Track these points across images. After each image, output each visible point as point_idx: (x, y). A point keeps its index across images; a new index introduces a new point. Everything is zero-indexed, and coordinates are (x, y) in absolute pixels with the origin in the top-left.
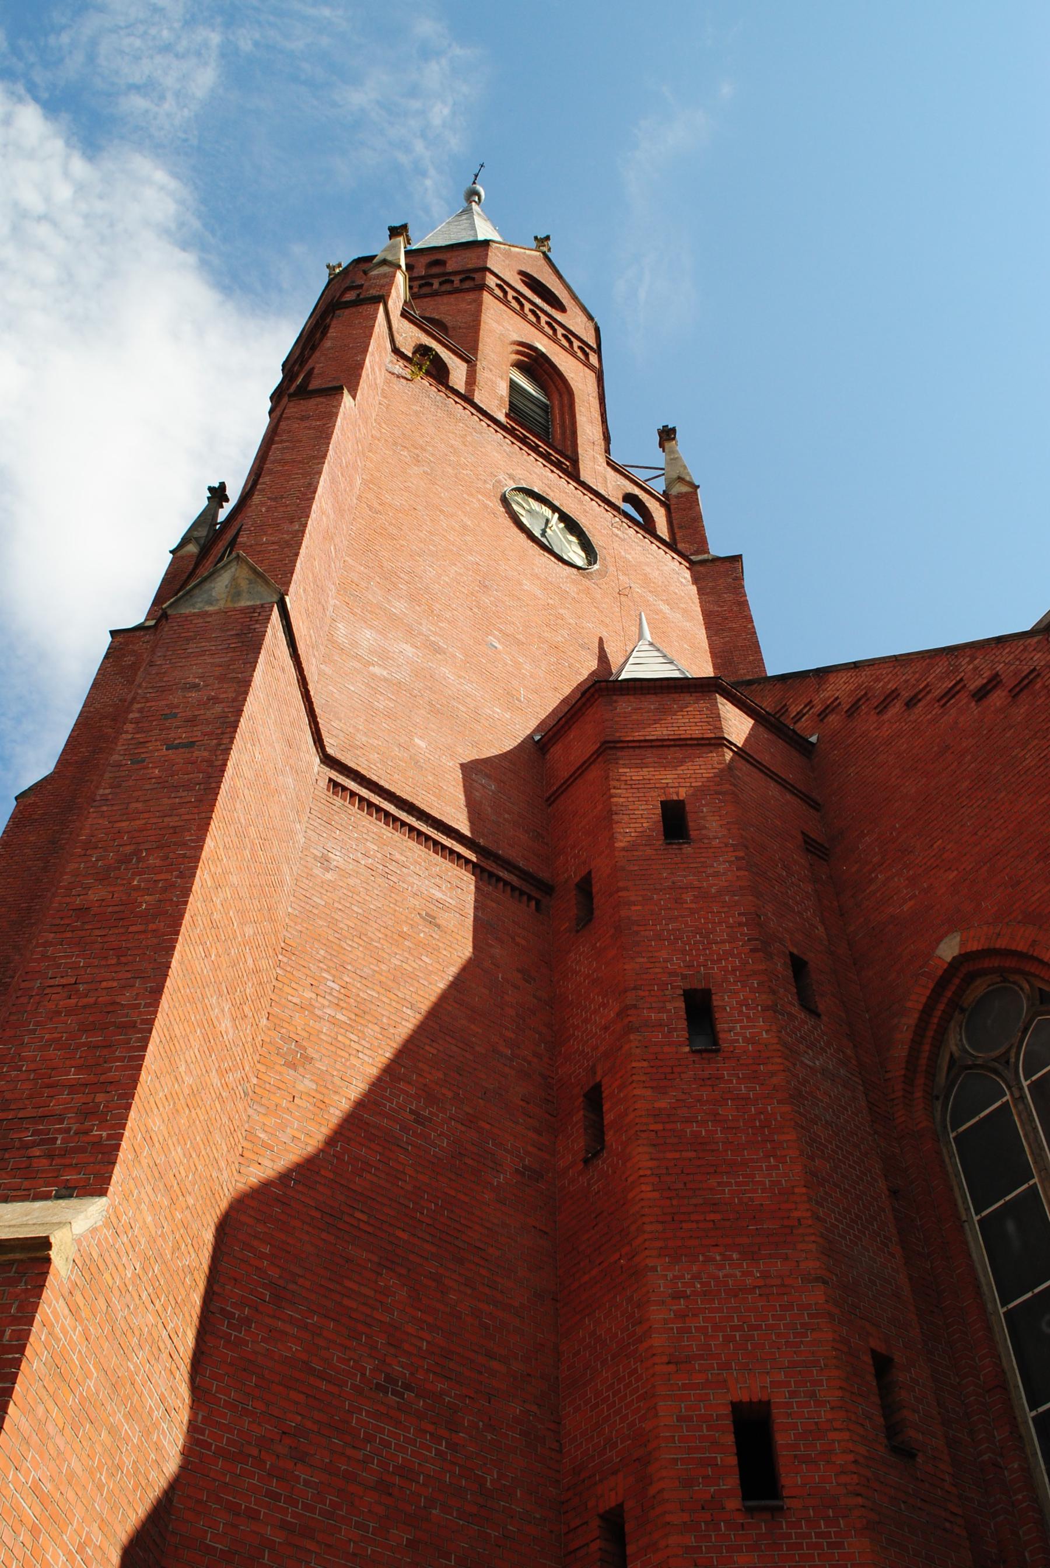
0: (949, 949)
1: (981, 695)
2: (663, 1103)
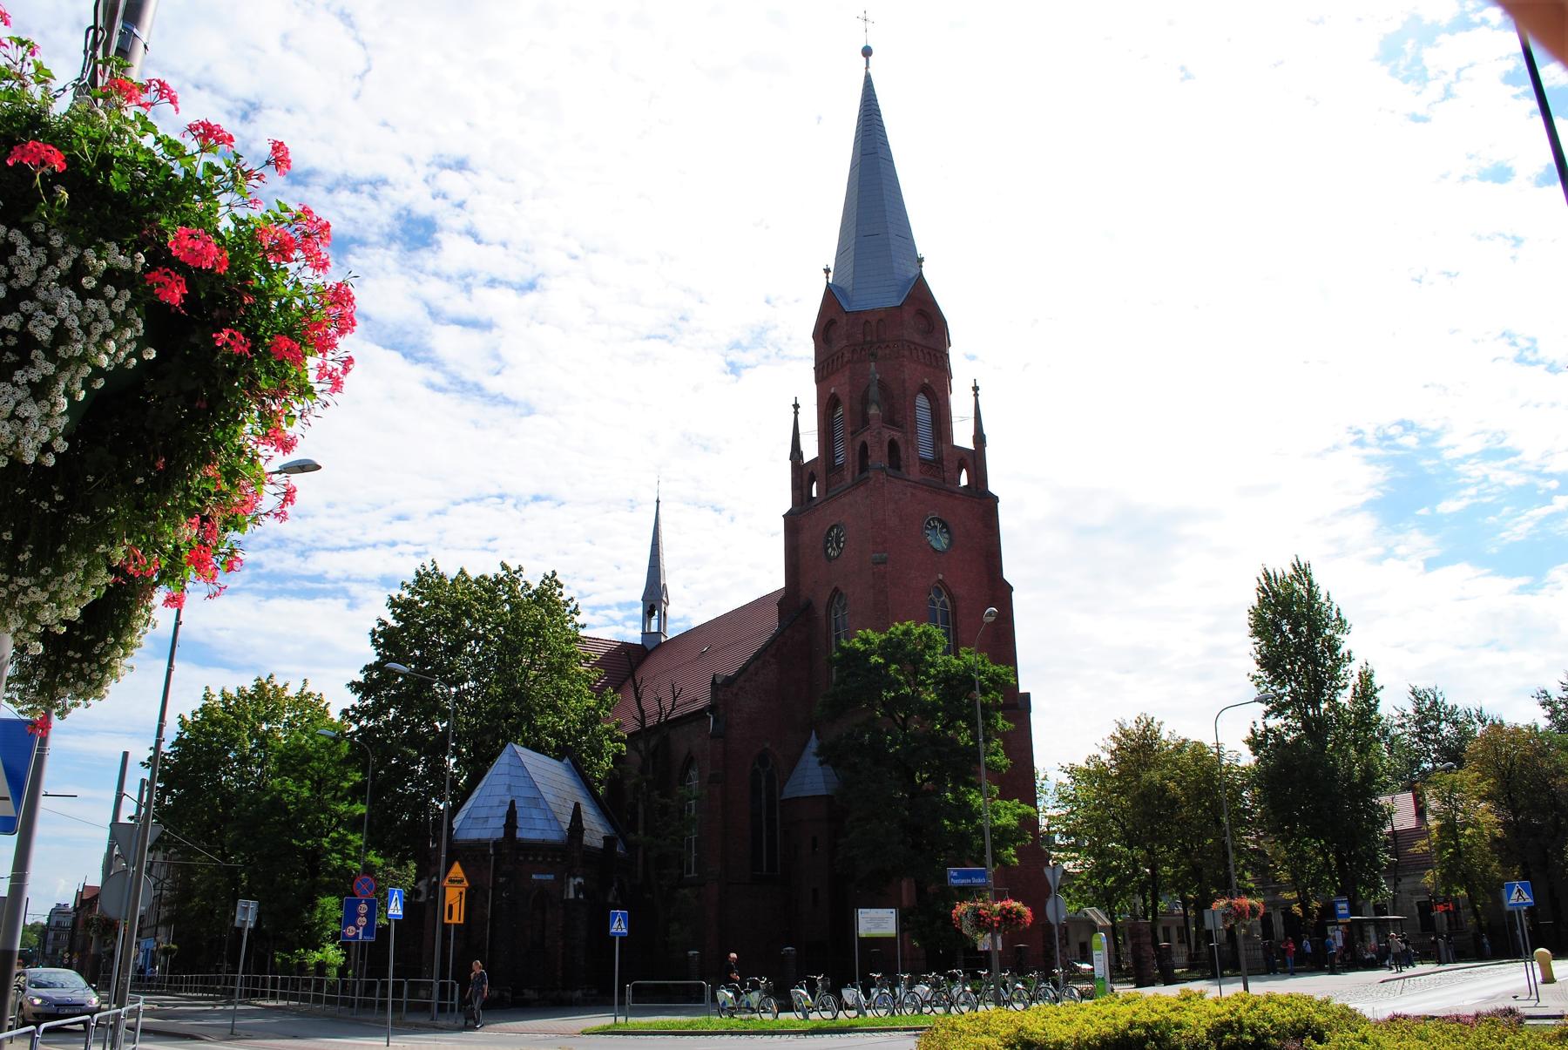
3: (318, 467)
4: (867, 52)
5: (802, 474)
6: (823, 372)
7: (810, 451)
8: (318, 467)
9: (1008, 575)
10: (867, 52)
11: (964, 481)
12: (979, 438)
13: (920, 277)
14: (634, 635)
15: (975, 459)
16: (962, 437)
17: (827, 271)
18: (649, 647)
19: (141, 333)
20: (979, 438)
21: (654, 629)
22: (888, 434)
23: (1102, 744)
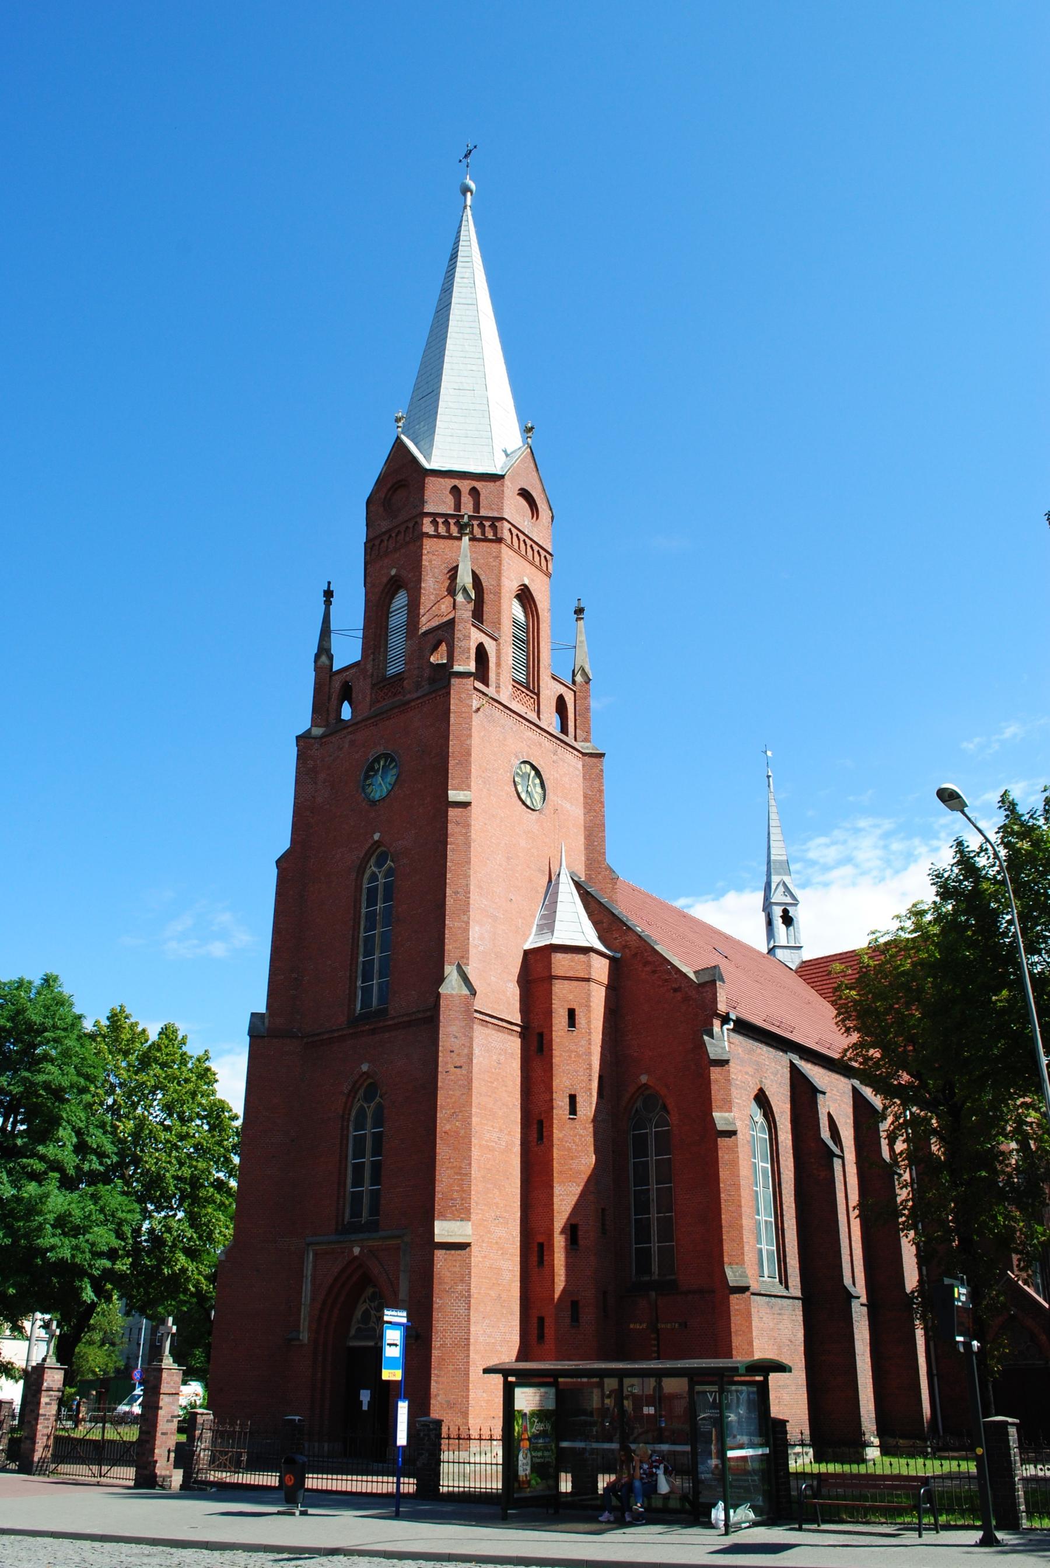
0: (644, 1079)
1: (675, 990)
2: (561, 1135)
5: (331, 687)
7: (347, 651)
22: (476, 637)
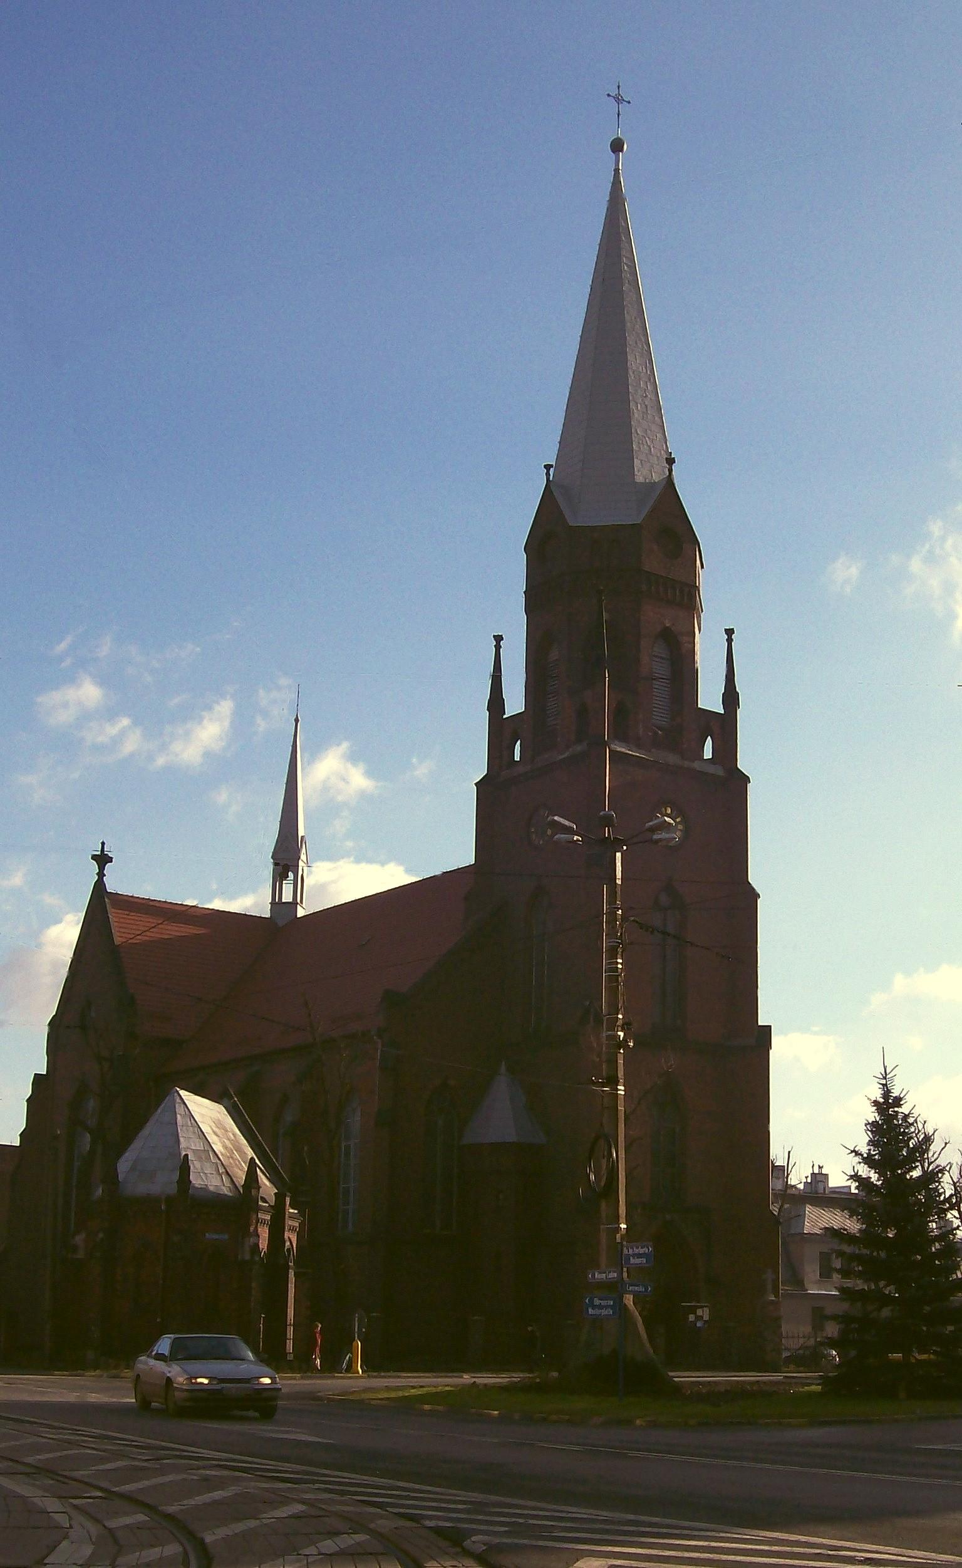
3: (888, 1104)
4: (617, 146)
5: (502, 730)
6: (537, 599)
7: (515, 704)
8: (888, 1104)
9: (755, 877)
10: (617, 146)
11: (708, 753)
12: (731, 697)
13: (670, 483)
14: (253, 901)
15: (725, 726)
16: (710, 698)
17: (548, 467)
18: (281, 923)
19: (125, 722)
20: (731, 697)
21: (287, 897)
23: (916, 1113)
